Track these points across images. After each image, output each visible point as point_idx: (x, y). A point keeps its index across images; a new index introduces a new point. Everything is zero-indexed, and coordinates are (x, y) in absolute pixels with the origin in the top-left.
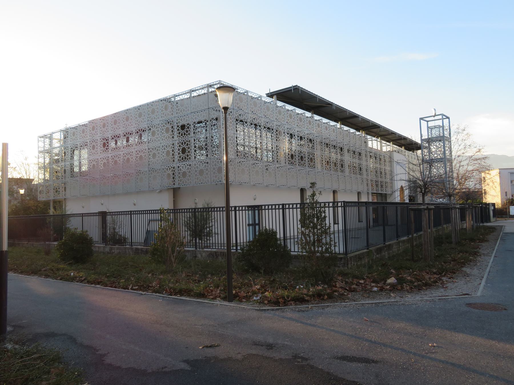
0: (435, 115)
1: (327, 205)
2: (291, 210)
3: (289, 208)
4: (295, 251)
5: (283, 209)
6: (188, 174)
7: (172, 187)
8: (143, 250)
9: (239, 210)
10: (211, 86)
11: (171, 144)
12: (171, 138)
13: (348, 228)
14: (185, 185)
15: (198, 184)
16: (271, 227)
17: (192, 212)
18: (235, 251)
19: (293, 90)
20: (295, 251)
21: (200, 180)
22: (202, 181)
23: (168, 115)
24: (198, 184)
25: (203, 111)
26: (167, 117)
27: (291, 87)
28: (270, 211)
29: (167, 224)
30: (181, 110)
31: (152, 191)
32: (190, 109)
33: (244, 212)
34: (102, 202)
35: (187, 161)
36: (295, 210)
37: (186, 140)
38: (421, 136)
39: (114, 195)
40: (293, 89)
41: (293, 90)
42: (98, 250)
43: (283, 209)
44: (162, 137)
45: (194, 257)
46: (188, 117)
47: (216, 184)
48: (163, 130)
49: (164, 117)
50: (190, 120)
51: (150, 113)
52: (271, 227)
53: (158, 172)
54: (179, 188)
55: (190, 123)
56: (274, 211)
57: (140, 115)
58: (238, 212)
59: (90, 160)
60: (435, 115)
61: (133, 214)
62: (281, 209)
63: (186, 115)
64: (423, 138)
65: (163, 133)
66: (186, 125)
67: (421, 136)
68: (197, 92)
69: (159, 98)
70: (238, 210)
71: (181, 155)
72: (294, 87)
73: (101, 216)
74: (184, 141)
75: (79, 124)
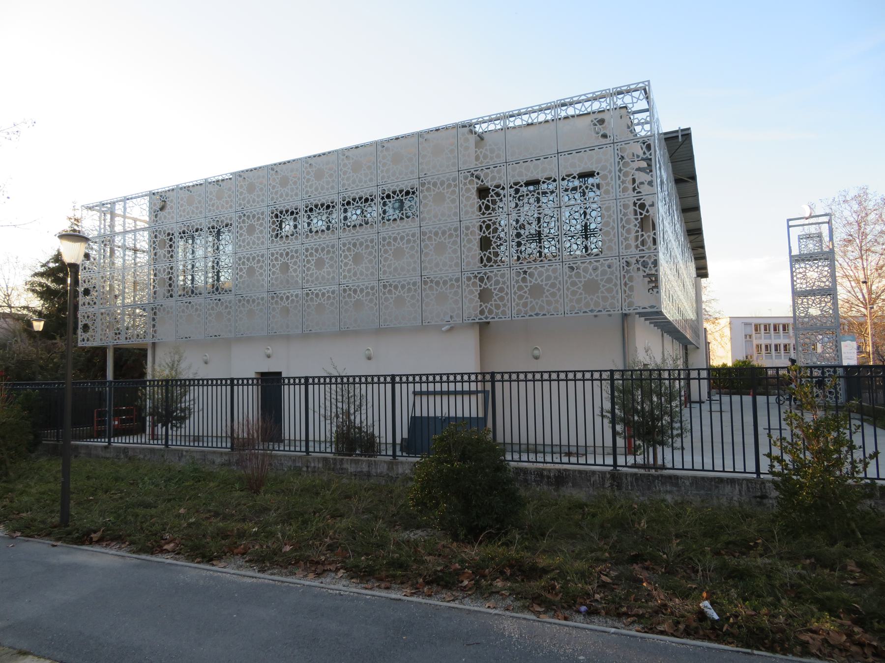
0: (811, 217)
1: (187, 383)
2: (363, 386)
3: (401, 383)
4: (316, 450)
5: (307, 384)
6: (368, 305)
7: (477, 320)
8: (545, 473)
9: (401, 383)
10: (103, 204)
11: (168, 268)
12: (168, 258)
13: (726, 417)
14: (537, 314)
15: (581, 314)
16: (445, 410)
17: (162, 386)
18: (612, 468)
19: (680, 137)
20: (316, 450)
21: (533, 308)
22: (537, 311)
23: (287, 195)
24: (581, 314)
25: (491, 167)
26: (357, 186)
27: (677, 131)
28: (219, 387)
29: (179, 405)
30: (188, 212)
31: (424, 327)
32: (204, 211)
33: (250, 387)
34: (269, 352)
35: (495, 267)
36: (382, 386)
37: (324, 244)
38: (790, 252)
39: (288, 338)
40: (682, 135)
41: (680, 137)
42: (369, 472)
43: (307, 384)
44: (239, 241)
45: (756, 497)
46: (499, 172)
47: (596, 316)
48: (241, 228)
49: (214, 211)
50: (505, 177)
51: (312, 178)
52: (445, 410)
53: (259, 303)
54: (488, 323)
55: (502, 185)
56: (214, 387)
57: (251, 188)
58: (235, 388)
59: (240, 259)
60: (811, 217)
61: (238, 385)
62: (605, 380)
63: (491, 167)
64: (792, 254)
65: (241, 235)
66: (492, 188)
67: (790, 252)
68: (578, 106)
69: (150, 189)
70: (398, 383)
71: (314, 271)
72: (683, 130)
73: (260, 387)
74: (251, 254)
75: (206, 180)
